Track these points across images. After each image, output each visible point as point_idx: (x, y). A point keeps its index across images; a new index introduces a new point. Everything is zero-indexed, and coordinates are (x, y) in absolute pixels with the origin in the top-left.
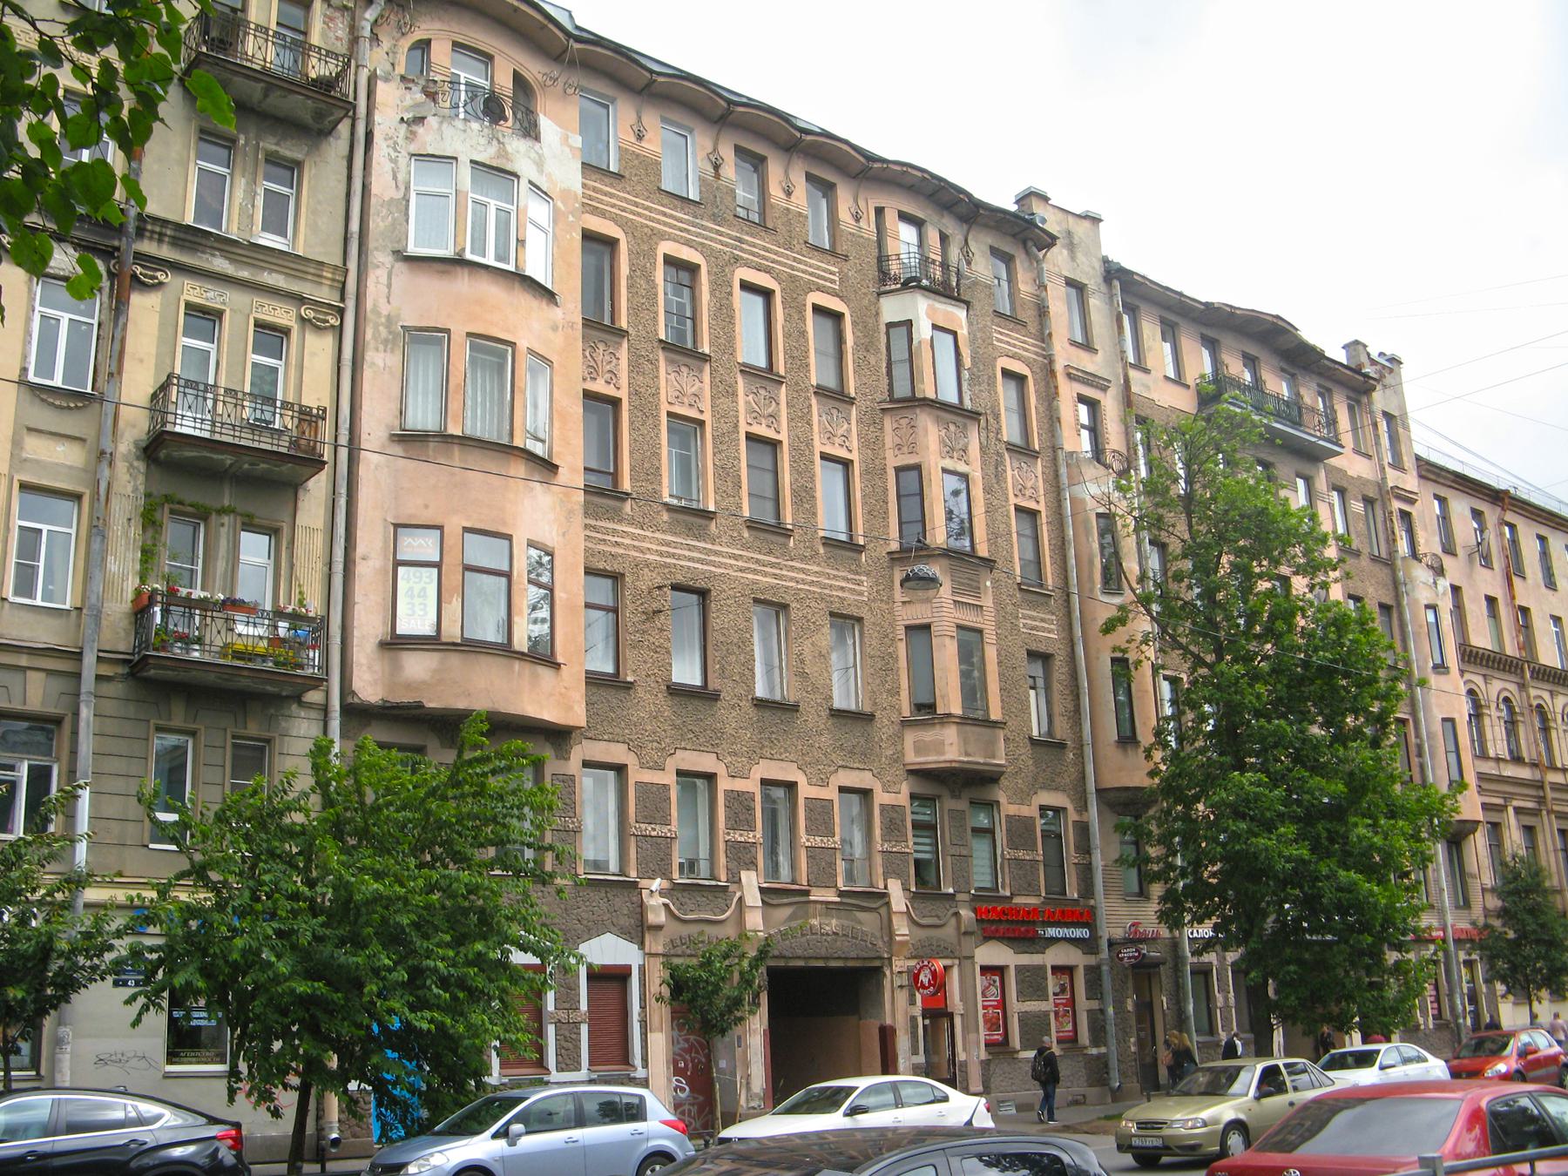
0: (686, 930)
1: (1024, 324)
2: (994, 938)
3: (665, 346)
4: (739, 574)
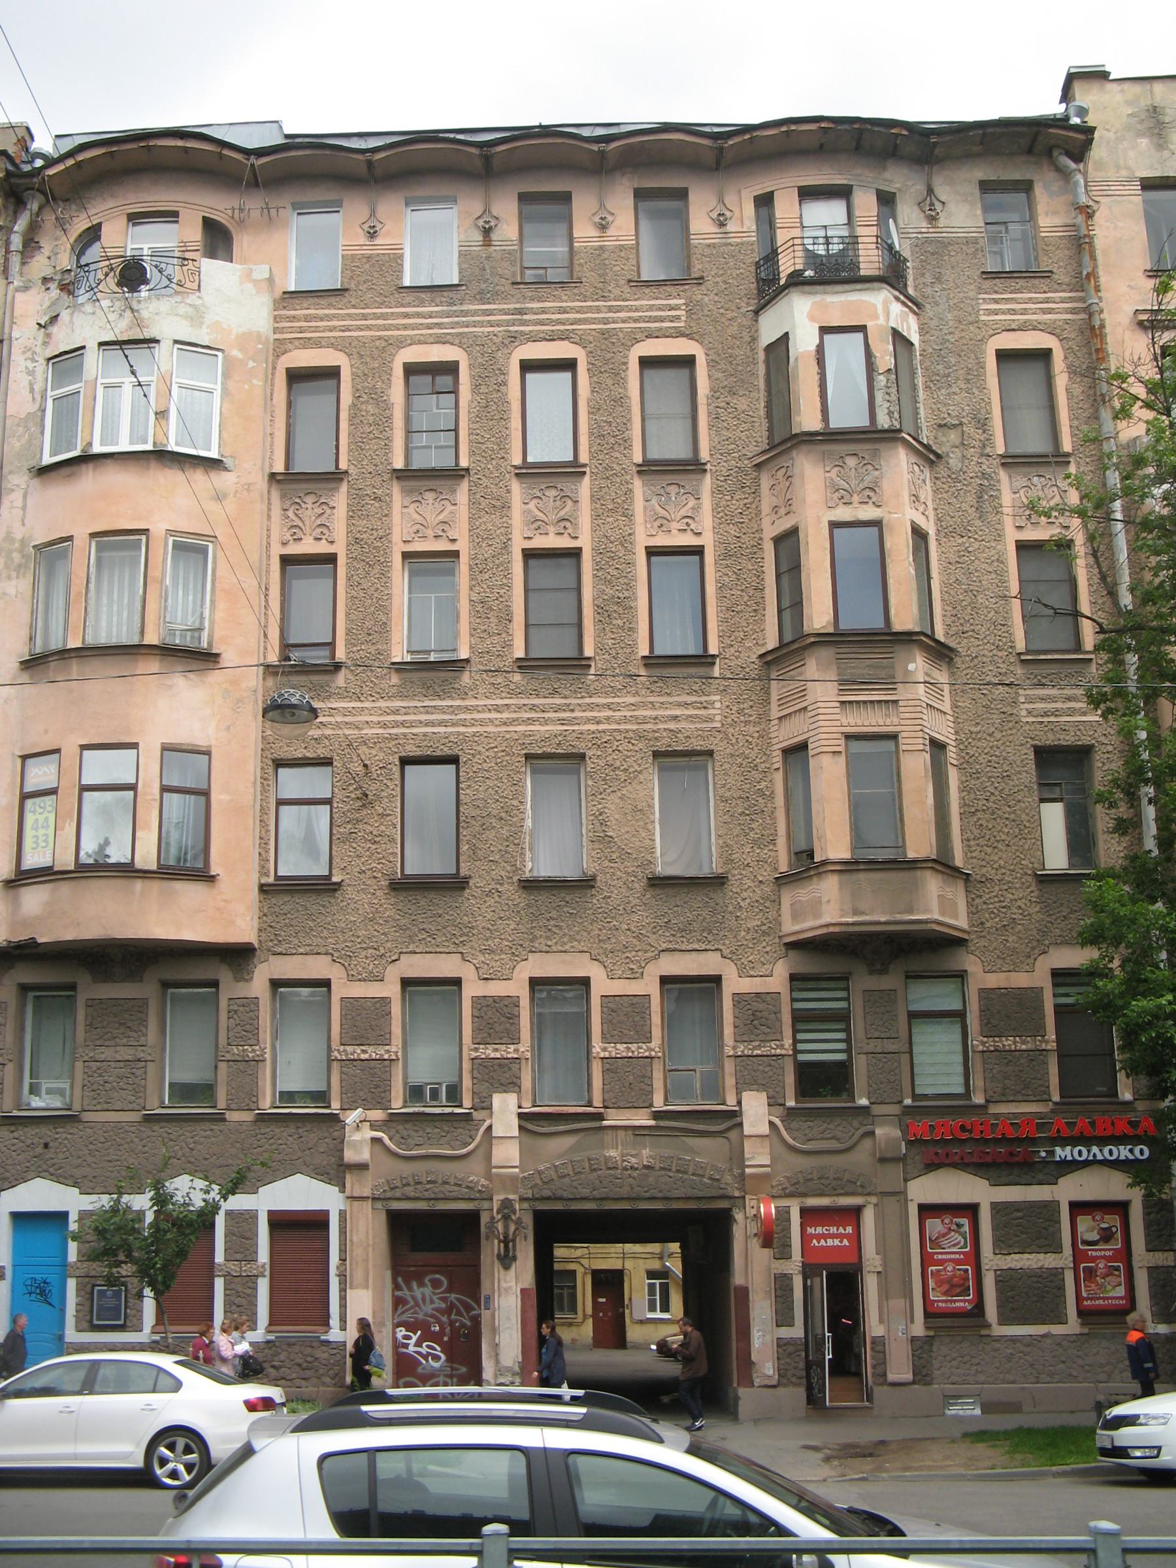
0: (407, 1169)
1: (1047, 275)
2: (948, 1165)
3: (401, 475)
4: (504, 729)
